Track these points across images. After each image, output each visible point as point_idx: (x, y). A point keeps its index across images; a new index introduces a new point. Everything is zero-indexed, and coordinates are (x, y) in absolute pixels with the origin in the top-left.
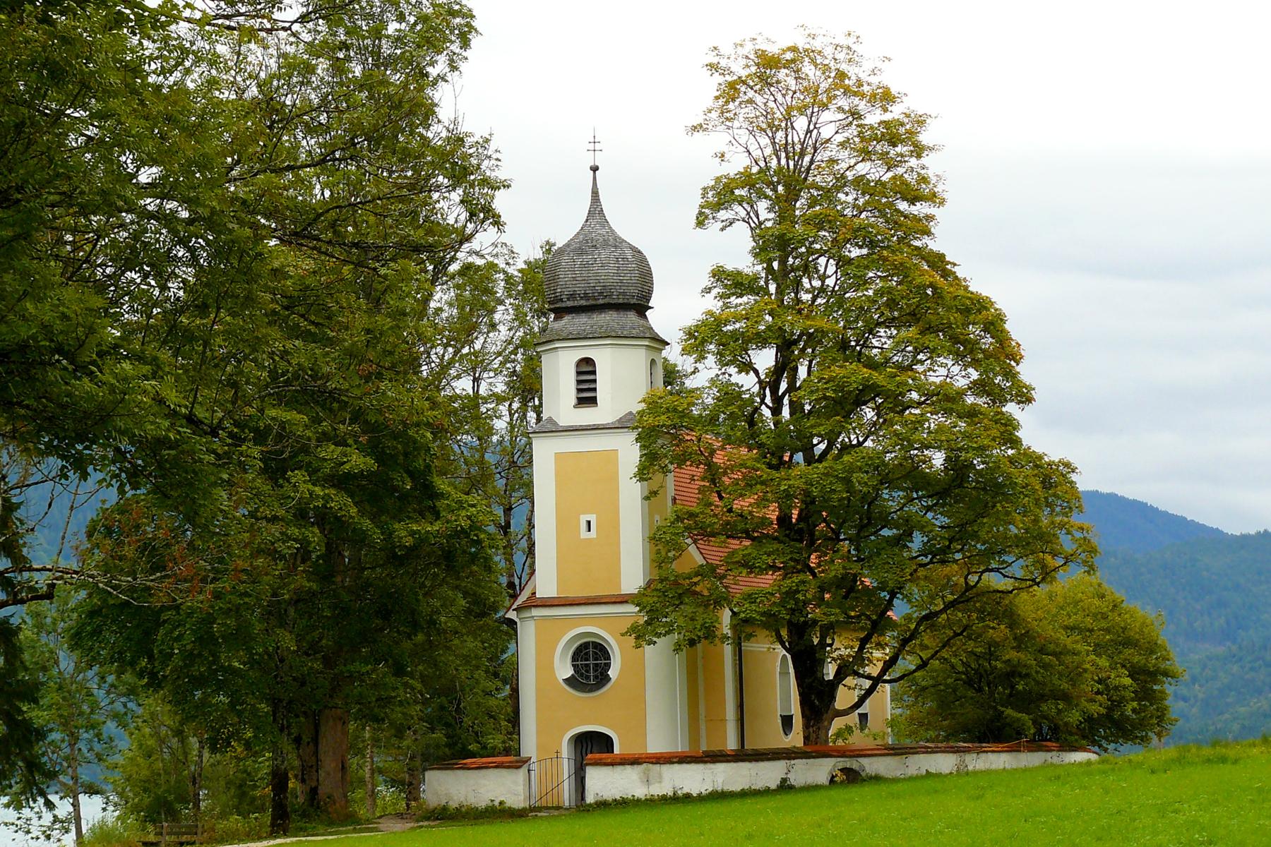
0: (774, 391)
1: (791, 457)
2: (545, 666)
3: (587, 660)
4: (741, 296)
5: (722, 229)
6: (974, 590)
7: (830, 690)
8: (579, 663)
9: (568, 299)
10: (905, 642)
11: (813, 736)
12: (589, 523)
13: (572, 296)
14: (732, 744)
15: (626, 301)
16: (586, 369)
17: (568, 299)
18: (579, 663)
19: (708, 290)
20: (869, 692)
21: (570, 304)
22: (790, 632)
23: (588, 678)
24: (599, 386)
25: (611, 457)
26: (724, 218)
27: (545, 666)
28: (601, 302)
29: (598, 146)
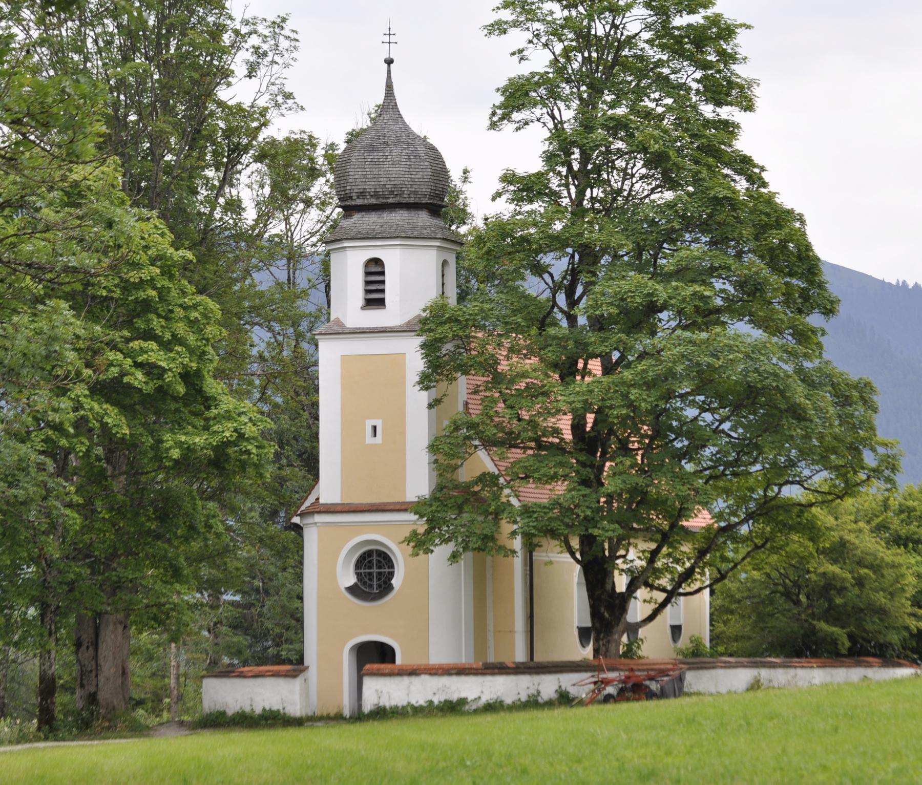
0: (570, 293)
1: (586, 364)
2: (327, 575)
3: (370, 568)
4: (531, 201)
5: (518, 129)
6: (773, 503)
7: (621, 602)
8: (362, 571)
9: (358, 197)
10: (701, 553)
11: (603, 649)
12: (375, 428)
13: (362, 194)
14: (520, 656)
15: (417, 200)
16: (374, 269)
17: (358, 197)
18: (362, 571)
19: (498, 195)
20: (663, 605)
21: (360, 202)
22: (582, 543)
23: (371, 586)
24: (388, 287)
25: (398, 359)
26: (517, 120)
27: (327, 575)
28: (391, 200)
29: (393, 39)
